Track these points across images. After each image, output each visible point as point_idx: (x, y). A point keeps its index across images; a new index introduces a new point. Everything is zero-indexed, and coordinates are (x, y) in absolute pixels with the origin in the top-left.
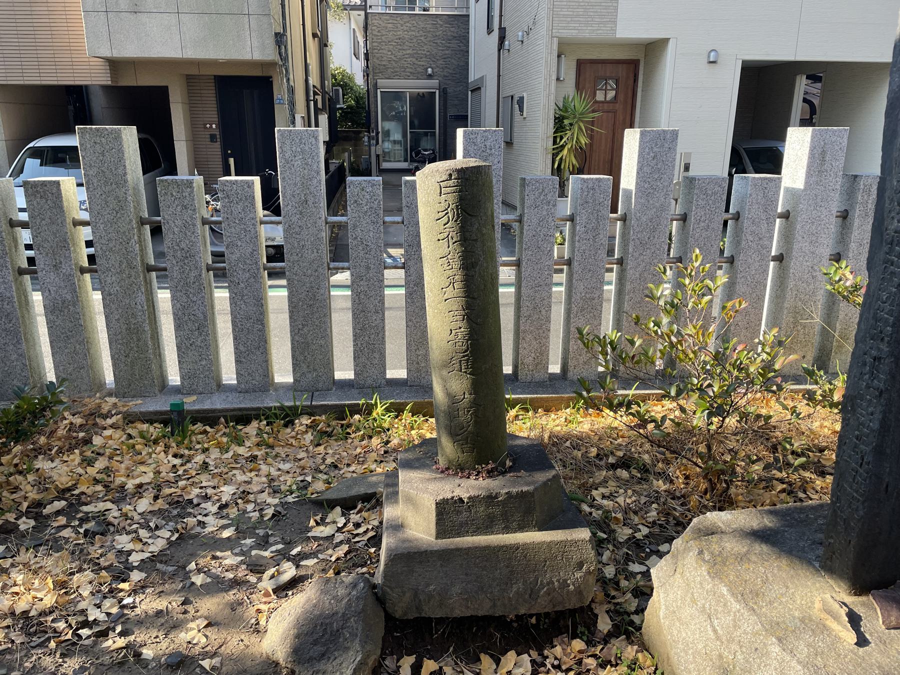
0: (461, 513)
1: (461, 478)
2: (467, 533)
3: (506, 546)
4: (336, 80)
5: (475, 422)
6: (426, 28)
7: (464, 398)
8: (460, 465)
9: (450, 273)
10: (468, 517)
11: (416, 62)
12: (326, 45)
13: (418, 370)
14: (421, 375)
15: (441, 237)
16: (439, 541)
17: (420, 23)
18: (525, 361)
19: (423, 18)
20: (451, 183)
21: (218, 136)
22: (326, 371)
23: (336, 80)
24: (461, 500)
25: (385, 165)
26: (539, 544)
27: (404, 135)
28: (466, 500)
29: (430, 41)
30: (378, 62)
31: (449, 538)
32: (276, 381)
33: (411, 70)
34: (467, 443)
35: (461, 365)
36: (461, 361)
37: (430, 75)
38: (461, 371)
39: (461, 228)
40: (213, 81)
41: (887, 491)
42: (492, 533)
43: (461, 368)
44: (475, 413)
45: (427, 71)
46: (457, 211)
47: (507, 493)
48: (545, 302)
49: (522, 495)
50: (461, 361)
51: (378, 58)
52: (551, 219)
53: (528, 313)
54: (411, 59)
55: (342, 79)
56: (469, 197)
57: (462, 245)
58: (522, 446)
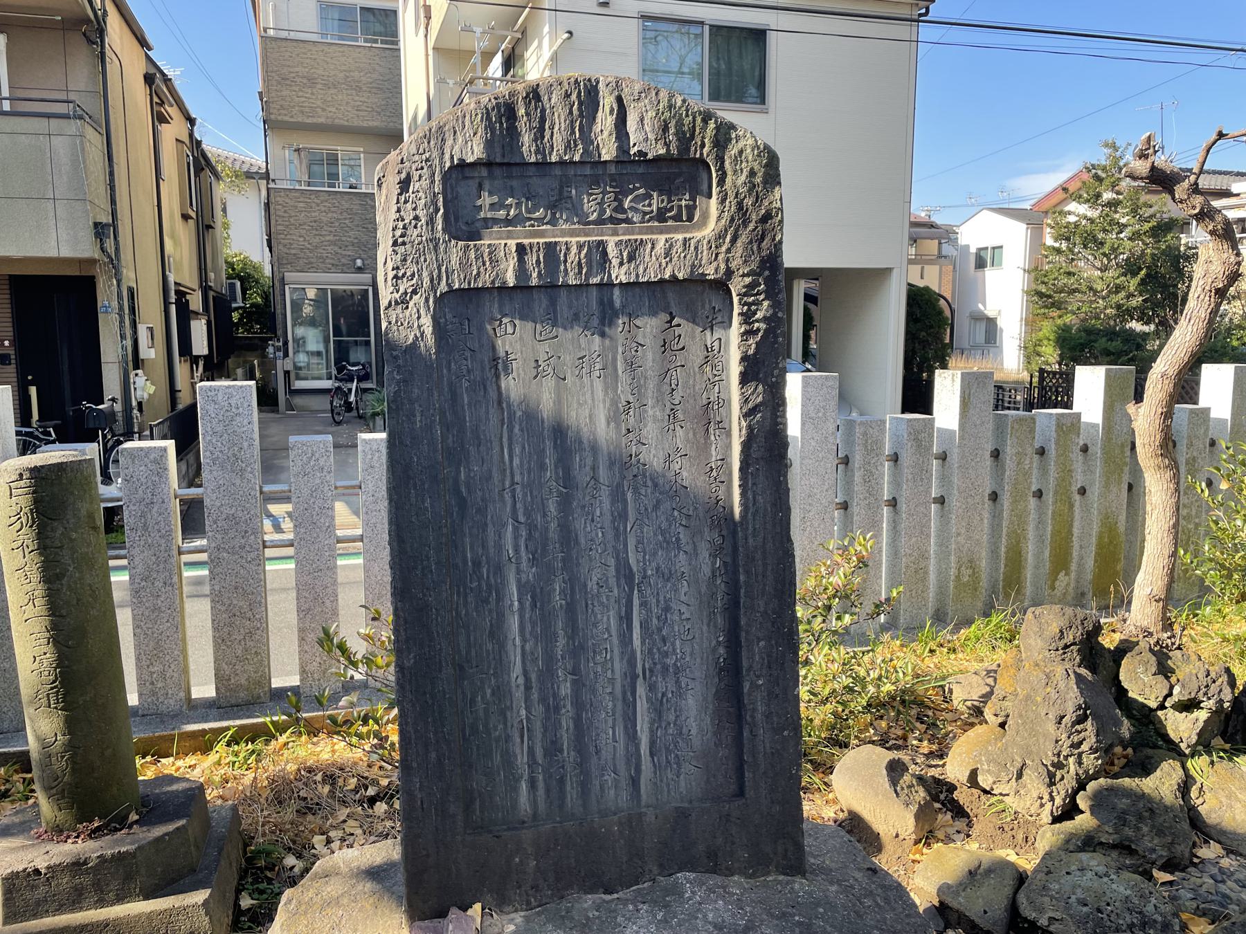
0: (37, 887)
1: (58, 842)
2: (47, 913)
3: (92, 924)
4: (233, 269)
5: (73, 768)
6: (351, 209)
7: (56, 740)
8: (58, 826)
9: (28, 588)
10: (47, 892)
11: (339, 251)
12: (209, 227)
13: (154, 693)
14: (157, 700)
15: (15, 545)
16: (7, 927)
17: (343, 203)
18: (307, 669)
19: (346, 197)
20: (22, 483)
21: (13, 357)
22: (13, 704)
23: (233, 269)
24: (37, 872)
25: (299, 384)
26: (135, 916)
27: (326, 341)
28: (43, 871)
29: (358, 226)
30: (285, 250)
31: (21, 922)
32: (193, 697)
33: (331, 261)
34: (63, 797)
35: (49, 700)
36: (48, 695)
37: (359, 268)
38: (49, 707)
39: (38, 534)
40: (7, 282)
41: (423, 809)
42: (81, 909)
43: (49, 702)
44: (72, 758)
45: (355, 263)
46: (32, 514)
47: (98, 857)
48: (330, 590)
49: (119, 858)
50: (48, 695)
51: (285, 246)
52: (326, 488)
53: (307, 606)
54: (332, 247)
55: (243, 269)
56: (47, 499)
57: (41, 554)
58: (176, 794)
